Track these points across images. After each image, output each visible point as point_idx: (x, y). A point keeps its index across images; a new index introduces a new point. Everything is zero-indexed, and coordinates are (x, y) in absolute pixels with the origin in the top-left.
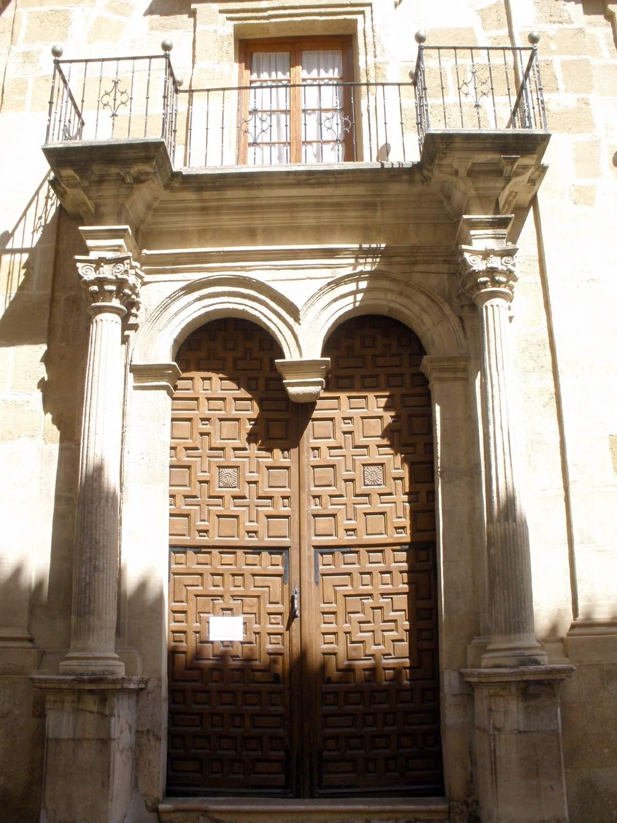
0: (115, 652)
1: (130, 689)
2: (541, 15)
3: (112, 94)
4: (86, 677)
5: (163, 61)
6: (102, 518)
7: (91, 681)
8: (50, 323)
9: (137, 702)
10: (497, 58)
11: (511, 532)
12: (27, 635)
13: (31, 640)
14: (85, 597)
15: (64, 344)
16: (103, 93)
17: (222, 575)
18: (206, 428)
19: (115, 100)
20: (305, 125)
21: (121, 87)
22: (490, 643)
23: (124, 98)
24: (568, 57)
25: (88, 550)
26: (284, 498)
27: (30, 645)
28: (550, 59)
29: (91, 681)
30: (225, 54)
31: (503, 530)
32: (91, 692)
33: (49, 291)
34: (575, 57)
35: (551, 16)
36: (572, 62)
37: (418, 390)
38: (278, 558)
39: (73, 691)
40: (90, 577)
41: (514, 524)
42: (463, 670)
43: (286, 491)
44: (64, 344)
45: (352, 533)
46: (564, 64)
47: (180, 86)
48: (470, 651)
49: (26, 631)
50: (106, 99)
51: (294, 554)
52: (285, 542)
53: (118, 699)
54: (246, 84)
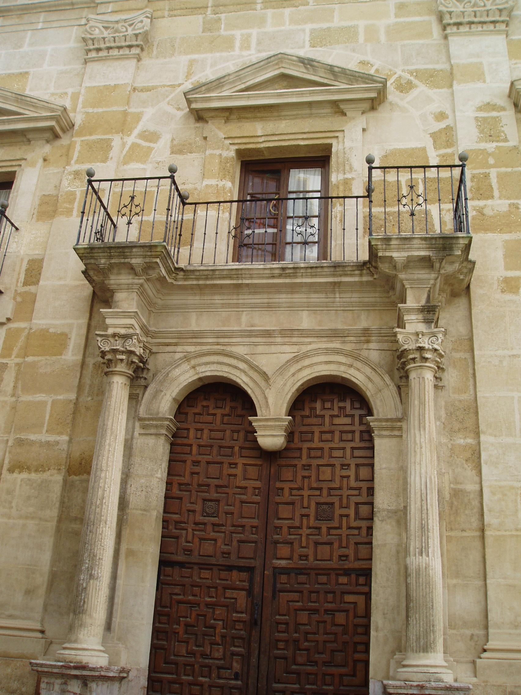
0: (102, 646)
1: (110, 677)
2: (482, 135)
3: (129, 206)
4: (72, 664)
5: (169, 181)
6: (100, 537)
7: (76, 668)
8: (80, 382)
9: (120, 688)
10: (445, 174)
11: (424, 565)
12: (39, 628)
13: (42, 632)
14: (81, 599)
15: (90, 398)
16: (122, 206)
17: (200, 586)
18: (196, 469)
19: (131, 211)
20: (331, 230)
21: (136, 201)
22: (404, 659)
23: (138, 210)
24: (503, 170)
25: (87, 561)
26: (252, 527)
27: (40, 635)
28: (487, 171)
29: (76, 668)
30: (227, 173)
31: (417, 563)
32: (76, 677)
33: (80, 357)
34: (509, 170)
35: (490, 136)
36: (506, 174)
37: (367, 444)
38: (244, 575)
39: (63, 675)
40: (87, 585)
41: (427, 558)
42: (385, 682)
43: (255, 522)
44: (90, 398)
45: (304, 558)
46: (500, 177)
47: (186, 199)
48: (392, 663)
49: (39, 624)
50: (124, 211)
51: (258, 572)
52: (252, 563)
53: (97, 685)
54: (232, 195)
